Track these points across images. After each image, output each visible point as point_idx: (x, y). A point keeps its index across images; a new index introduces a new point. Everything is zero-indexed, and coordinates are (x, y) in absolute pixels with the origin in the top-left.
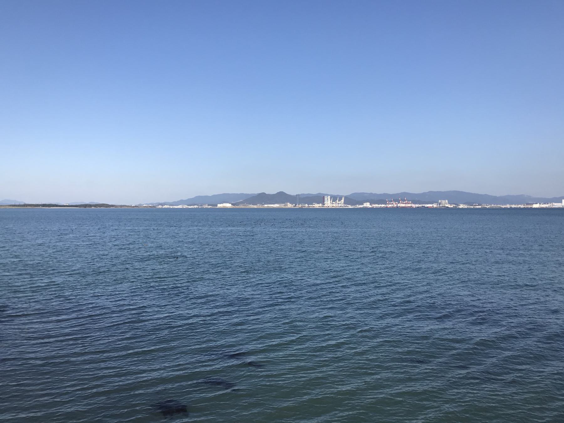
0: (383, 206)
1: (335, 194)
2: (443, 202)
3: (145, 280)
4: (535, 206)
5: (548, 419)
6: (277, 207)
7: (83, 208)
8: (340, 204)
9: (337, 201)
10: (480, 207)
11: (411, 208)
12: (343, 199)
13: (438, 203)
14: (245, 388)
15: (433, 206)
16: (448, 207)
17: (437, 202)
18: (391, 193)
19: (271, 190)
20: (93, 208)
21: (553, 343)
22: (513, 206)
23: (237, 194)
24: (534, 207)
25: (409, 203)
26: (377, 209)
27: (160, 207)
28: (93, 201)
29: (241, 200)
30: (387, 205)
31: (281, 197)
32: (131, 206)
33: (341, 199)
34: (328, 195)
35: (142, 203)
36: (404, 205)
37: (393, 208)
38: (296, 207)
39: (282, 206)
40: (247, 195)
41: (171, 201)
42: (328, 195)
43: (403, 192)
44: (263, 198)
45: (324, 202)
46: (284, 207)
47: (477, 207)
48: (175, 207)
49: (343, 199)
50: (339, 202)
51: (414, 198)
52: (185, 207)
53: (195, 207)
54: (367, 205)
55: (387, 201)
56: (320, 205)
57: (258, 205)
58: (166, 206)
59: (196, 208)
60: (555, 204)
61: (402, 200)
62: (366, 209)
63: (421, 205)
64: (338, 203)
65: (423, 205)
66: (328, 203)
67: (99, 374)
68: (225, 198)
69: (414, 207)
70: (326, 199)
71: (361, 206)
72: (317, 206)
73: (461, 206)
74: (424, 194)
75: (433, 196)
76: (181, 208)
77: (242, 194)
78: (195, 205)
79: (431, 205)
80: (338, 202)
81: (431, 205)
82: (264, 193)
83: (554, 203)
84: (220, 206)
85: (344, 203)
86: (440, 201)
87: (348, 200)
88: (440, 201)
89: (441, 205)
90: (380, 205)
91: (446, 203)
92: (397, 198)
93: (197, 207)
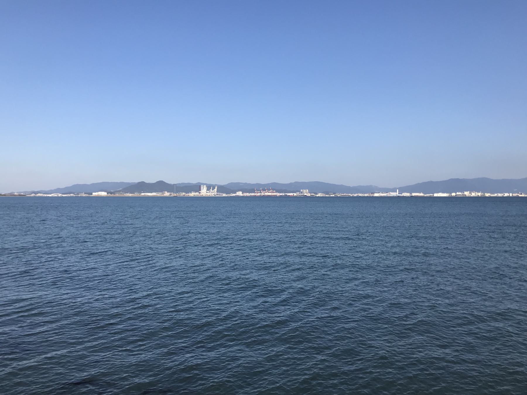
2: (305, 191)
4: (376, 195)
8: (213, 193)
9: (211, 190)
10: (334, 195)
11: (275, 197)
12: (216, 188)
13: (300, 191)
15: (294, 195)
17: (300, 191)
21: (152, 342)
22: (360, 195)
23: (117, 183)
25: (273, 192)
26: (247, 197)
27: (33, 195)
28: (32, 190)
29: (121, 189)
30: (518, 195)
31: (161, 186)
33: (215, 188)
34: (204, 184)
35: (14, 192)
36: (270, 194)
38: (171, 196)
39: (159, 194)
40: (129, 183)
42: (204, 184)
44: (142, 186)
45: (200, 190)
46: (162, 195)
47: (331, 195)
48: (48, 195)
49: (216, 188)
50: (212, 191)
51: (274, 187)
52: (60, 195)
53: (72, 195)
54: (240, 194)
56: (197, 193)
57: (136, 193)
58: (39, 195)
60: (392, 193)
61: (257, 190)
62: (238, 197)
63: (284, 194)
65: (286, 194)
66: (204, 192)
68: (100, 187)
69: (278, 196)
70: (202, 188)
71: (234, 195)
72: (192, 194)
73: (319, 195)
74: (290, 184)
75: (297, 186)
76: (55, 197)
78: (71, 193)
80: (211, 191)
84: (94, 194)
85: (217, 192)
87: (221, 189)
88: (302, 190)
89: (302, 194)
90: (250, 194)
91: (306, 193)
92: (265, 187)
93: (73, 195)
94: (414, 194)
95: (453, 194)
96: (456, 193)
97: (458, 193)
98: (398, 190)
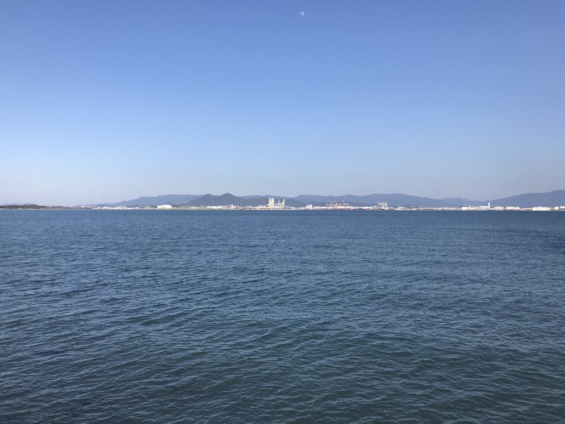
0: (324, 208)
1: (277, 195)
2: (383, 204)
3: (336, 283)
4: (464, 209)
5: (334, 403)
6: (221, 209)
7: (9, 209)
8: (281, 206)
9: (279, 203)
10: (415, 209)
11: (348, 210)
12: (284, 201)
14: (559, 378)
16: (384, 209)
17: (377, 205)
18: (336, 196)
19: (218, 192)
20: (20, 209)
22: (446, 209)
24: (462, 210)
29: (187, 202)
31: (227, 198)
32: (69, 208)
34: (271, 197)
37: (332, 210)
41: (113, 202)
42: (271, 197)
43: (514, 195)
44: (208, 199)
46: (228, 209)
47: (413, 209)
48: (113, 208)
49: (284, 201)
53: (137, 208)
54: (310, 207)
55: (326, 204)
58: (105, 208)
59: (138, 210)
63: (358, 208)
64: (280, 205)
65: (361, 207)
66: (271, 205)
67: (104, 408)
71: (304, 208)
75: (375, 199)
77: (188, 196)
79: (367, 208)
80: (279, 204)
81: (367, 208)
82: (210, 195)
83: (481, 206)
84: (159, 207)
85: (285, 205)
86: (379, 204)
87: (289, 202)
91: (385, 207)
94: (508, 208)
95: (557, 208)
96: (559, 207)
97: (561, 207)
98: (489, 204)
